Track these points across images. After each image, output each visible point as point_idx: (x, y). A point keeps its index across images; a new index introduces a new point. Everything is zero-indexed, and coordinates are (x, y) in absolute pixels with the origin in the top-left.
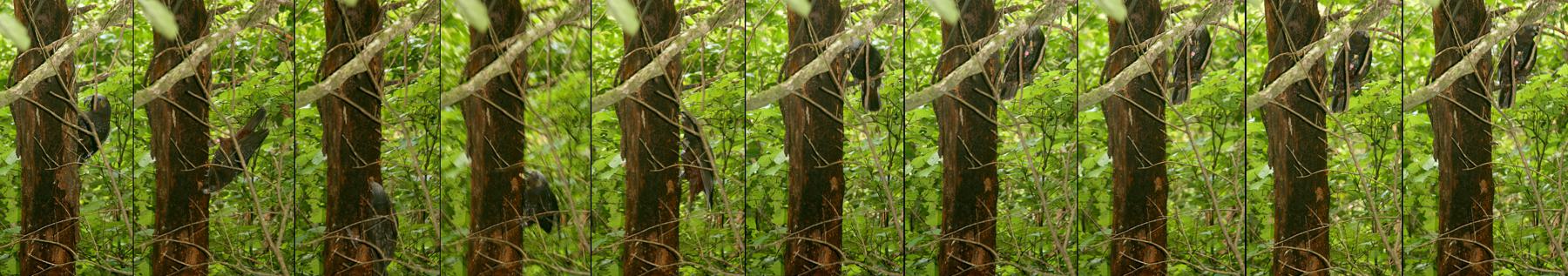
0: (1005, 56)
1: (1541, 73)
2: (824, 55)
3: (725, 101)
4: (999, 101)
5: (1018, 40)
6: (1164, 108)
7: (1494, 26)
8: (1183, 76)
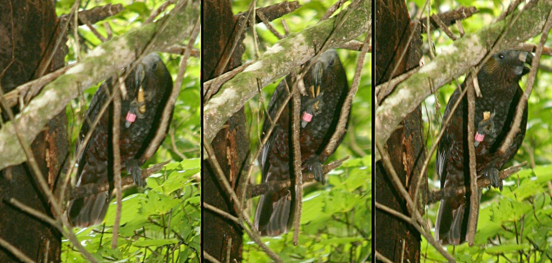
0: (79, 123)
1: (539, 163)
2: (16, 124)
3: (530, 231)
4: (65, 228)
5: (110, 87)
6: (239, 242)
7: (428, 53)
8: (285, 168)
